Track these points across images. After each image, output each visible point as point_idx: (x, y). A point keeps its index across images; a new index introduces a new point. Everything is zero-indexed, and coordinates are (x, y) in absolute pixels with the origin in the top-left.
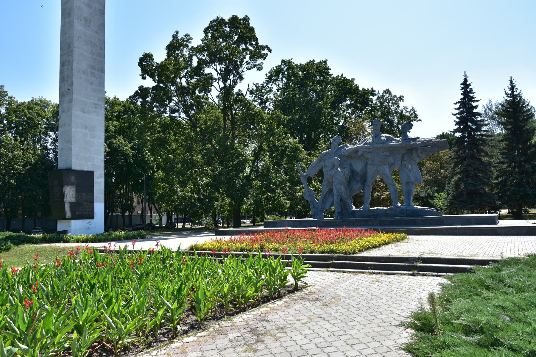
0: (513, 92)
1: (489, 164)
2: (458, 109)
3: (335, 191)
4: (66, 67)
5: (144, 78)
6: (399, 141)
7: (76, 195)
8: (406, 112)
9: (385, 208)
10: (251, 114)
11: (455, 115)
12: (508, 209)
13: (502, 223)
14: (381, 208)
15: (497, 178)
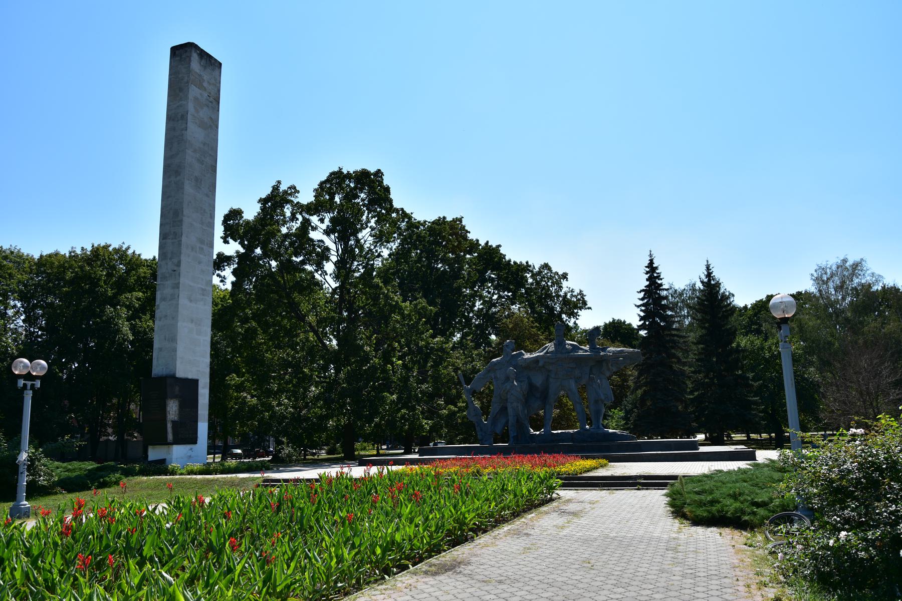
0: (709, 280)
1: (682, 373)
2: (642, 299)
3: (510, 410)
4: (169, 241)
5: (227, 242)
6: (586, 351)
7: (180, 412)
8: (572, 296)
9: (571, 431)
10: (390, 305)
11: (638, 306)
12: (705, 434)
13: (703, 449)
14: (567, 431)
15: (691, 393)
